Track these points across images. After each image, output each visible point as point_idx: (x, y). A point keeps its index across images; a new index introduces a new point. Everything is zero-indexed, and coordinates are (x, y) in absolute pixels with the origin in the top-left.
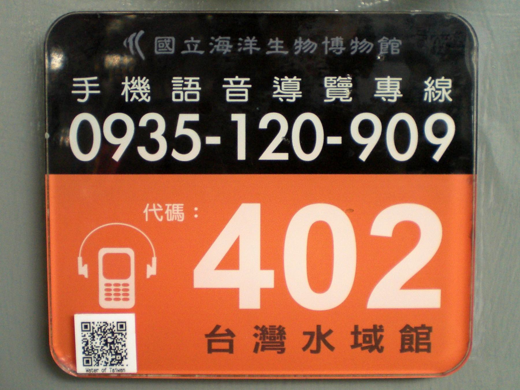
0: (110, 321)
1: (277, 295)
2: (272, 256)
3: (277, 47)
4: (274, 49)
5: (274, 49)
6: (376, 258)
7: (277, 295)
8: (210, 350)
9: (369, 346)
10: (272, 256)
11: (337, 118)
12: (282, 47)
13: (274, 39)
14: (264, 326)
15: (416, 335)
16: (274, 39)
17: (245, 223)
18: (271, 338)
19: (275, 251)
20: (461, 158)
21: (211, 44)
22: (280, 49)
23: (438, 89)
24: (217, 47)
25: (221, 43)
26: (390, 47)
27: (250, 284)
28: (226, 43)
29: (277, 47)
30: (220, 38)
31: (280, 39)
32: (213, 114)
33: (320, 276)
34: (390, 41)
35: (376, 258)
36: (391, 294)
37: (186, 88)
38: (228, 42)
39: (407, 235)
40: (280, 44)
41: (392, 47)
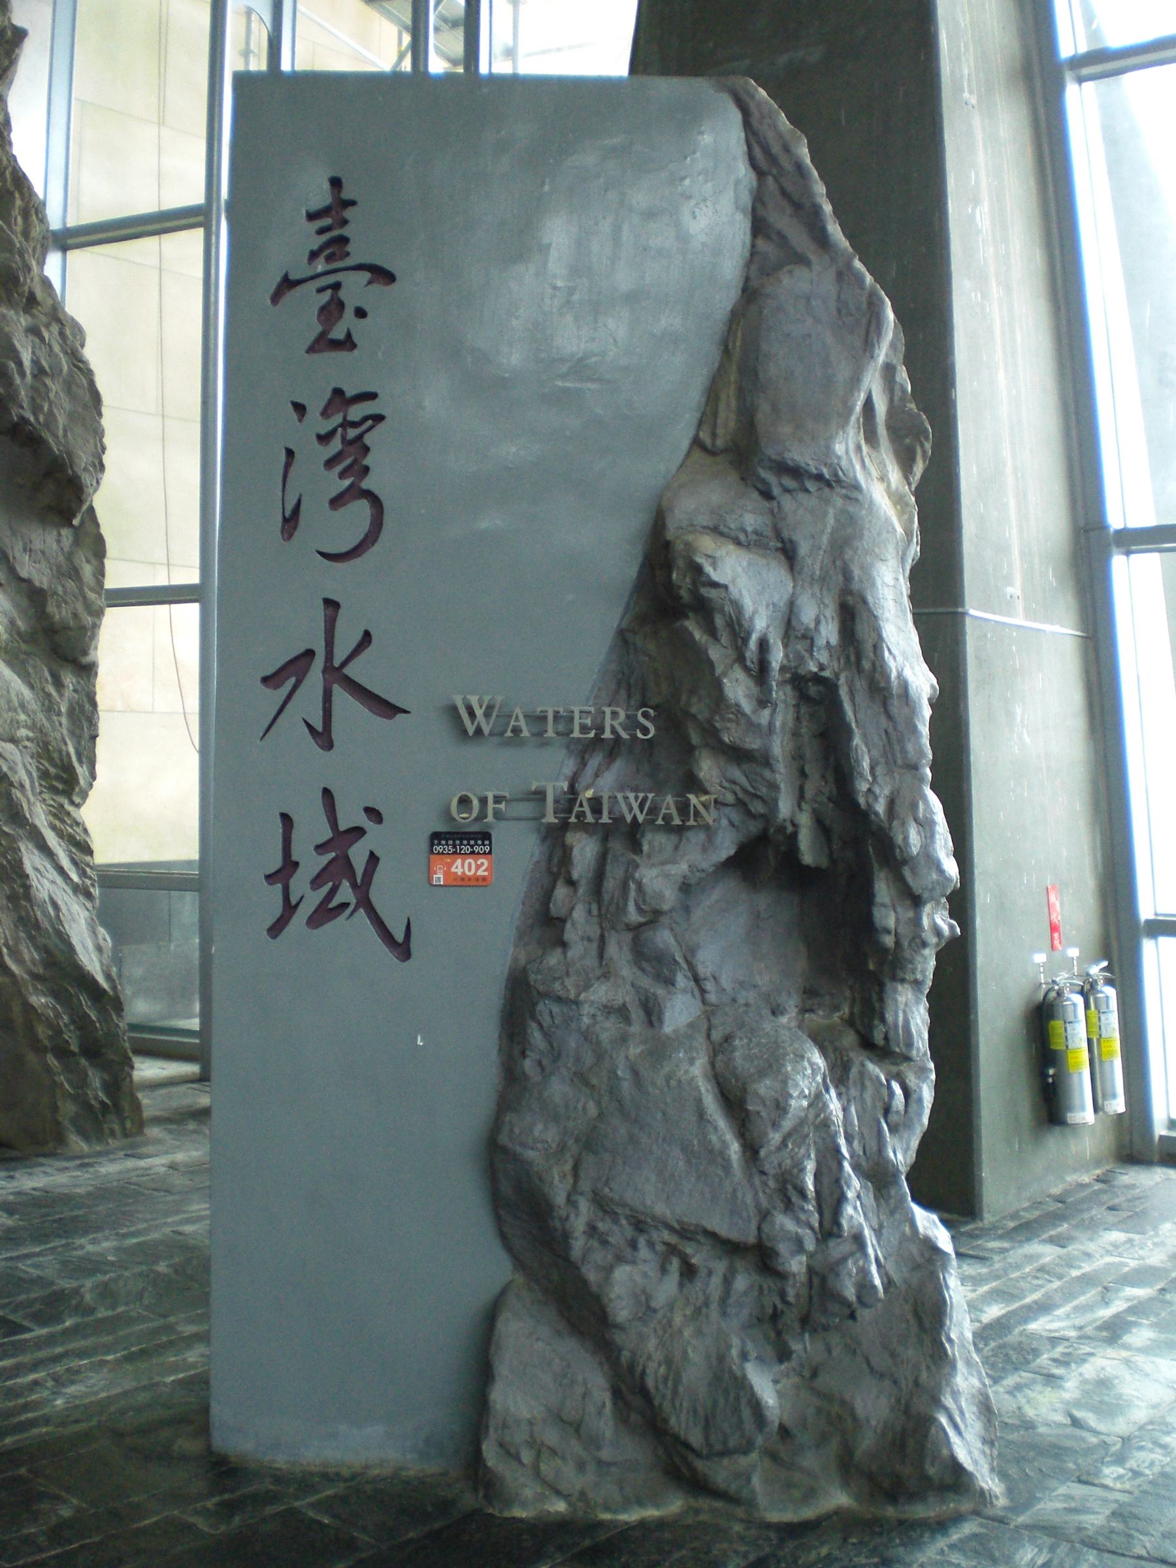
0: (439, 877)
1: (464, 873)
2: (463, 867)
6: (478, 867)
7: (464, 873)
8: (432, 852)
9: (19, 1414)
10: (463, 867)
11: (472, 847)
14: (366, 470)
15: (484, 878)
17: (459, 862)
18: (463, 879)
19: (463, 867)
20: (490, 852)
23: (487, 842)
27: (459, 871)
32: (454, 846)
33: (470, 870)
35: (478, 867)
36: (480, 873)
37: (451, 842)
39: (482, 864)
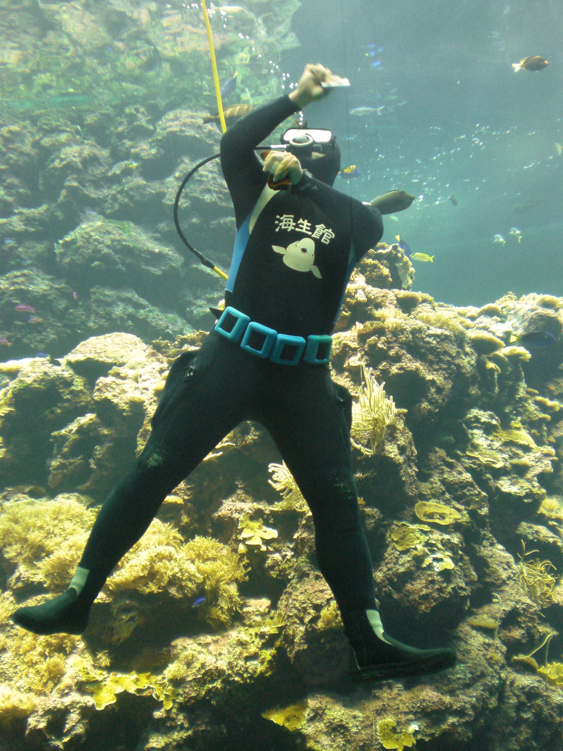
3: (305, 227)
4: (302, 228)
5: (302, 228)
12: (309, 228)
13: (304, 220)
16: (304, 220)
21: (277, 222)
22: (306, 230)
24: (282, 224)
25: (286, 221)
26: (323, 234)
28: (290, 221)
29: (305, 227)
30: (285, 216)
31: (308, 222)
34: (326, 230)
38: (292, 220)
40: (307, 226)
41: (325, 235)
